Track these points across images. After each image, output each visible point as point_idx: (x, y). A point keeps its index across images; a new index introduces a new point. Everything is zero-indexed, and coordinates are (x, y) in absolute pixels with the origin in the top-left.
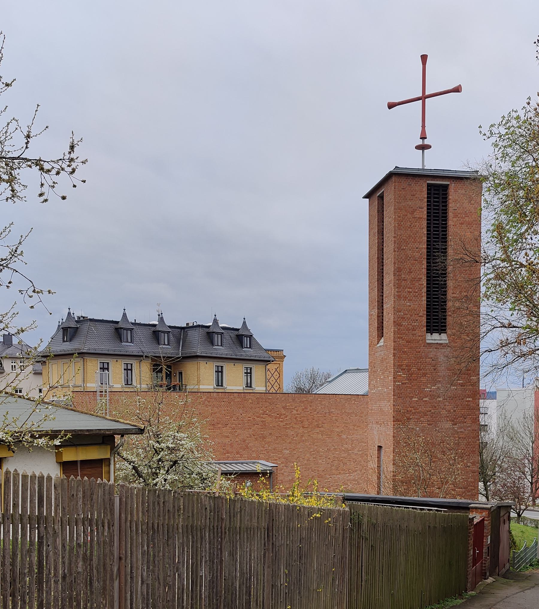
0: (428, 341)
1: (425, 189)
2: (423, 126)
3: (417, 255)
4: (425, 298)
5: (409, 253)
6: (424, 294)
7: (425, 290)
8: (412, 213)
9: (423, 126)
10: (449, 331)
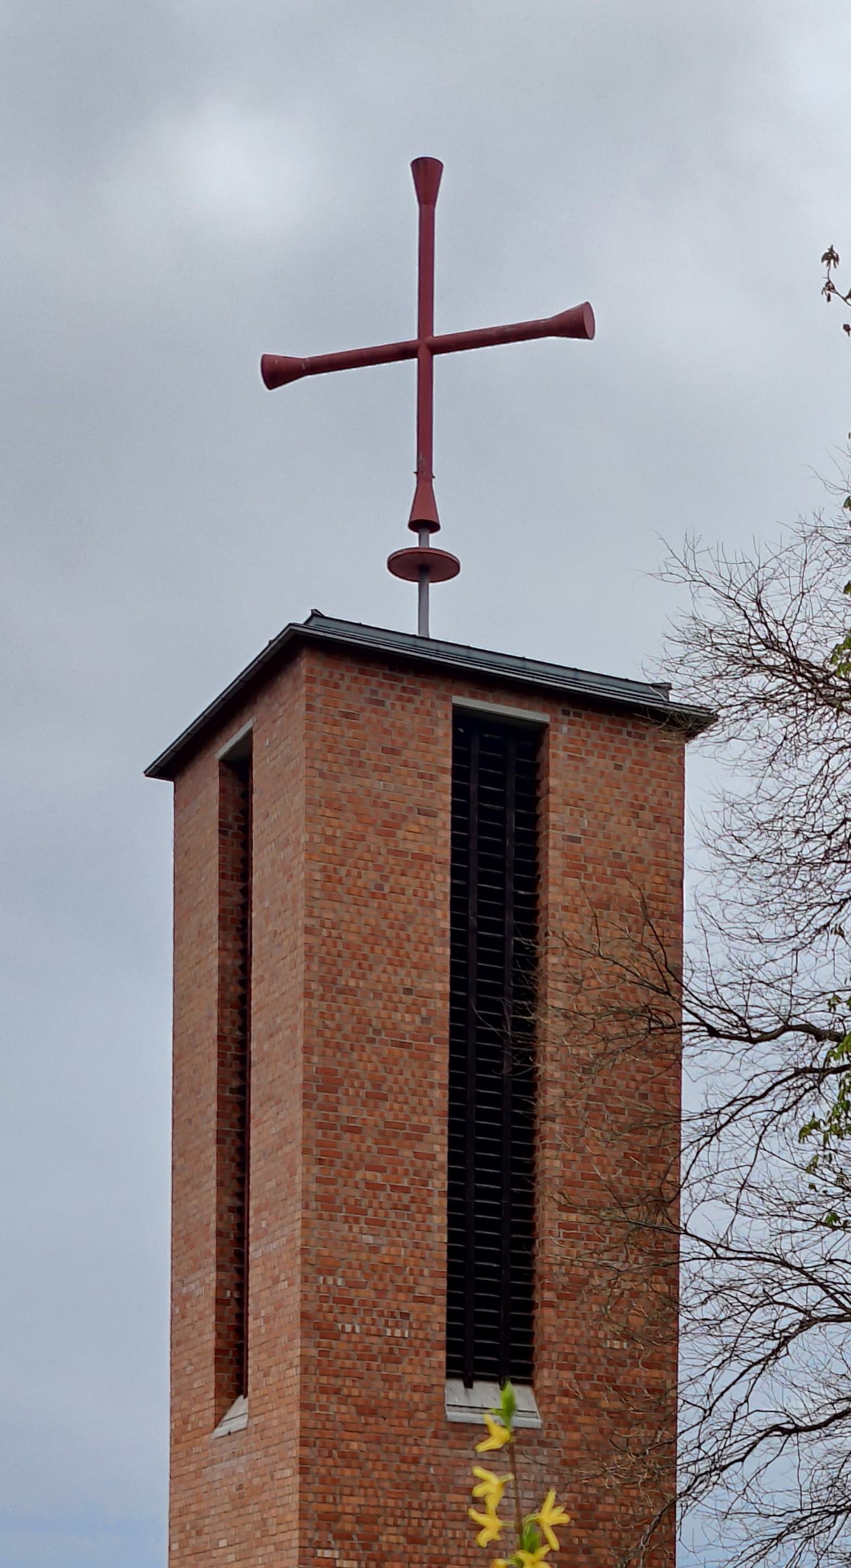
0: (453, 1415)
1: (444, 731)
2: (424, 473)
3: (407, 1023)
4: (440, 1220)
5: (374, 1008)
6: (439, 1202)
7: (440, 1182)
8: (389, 829)
9: (424, 473)
10: (545, 1378)
